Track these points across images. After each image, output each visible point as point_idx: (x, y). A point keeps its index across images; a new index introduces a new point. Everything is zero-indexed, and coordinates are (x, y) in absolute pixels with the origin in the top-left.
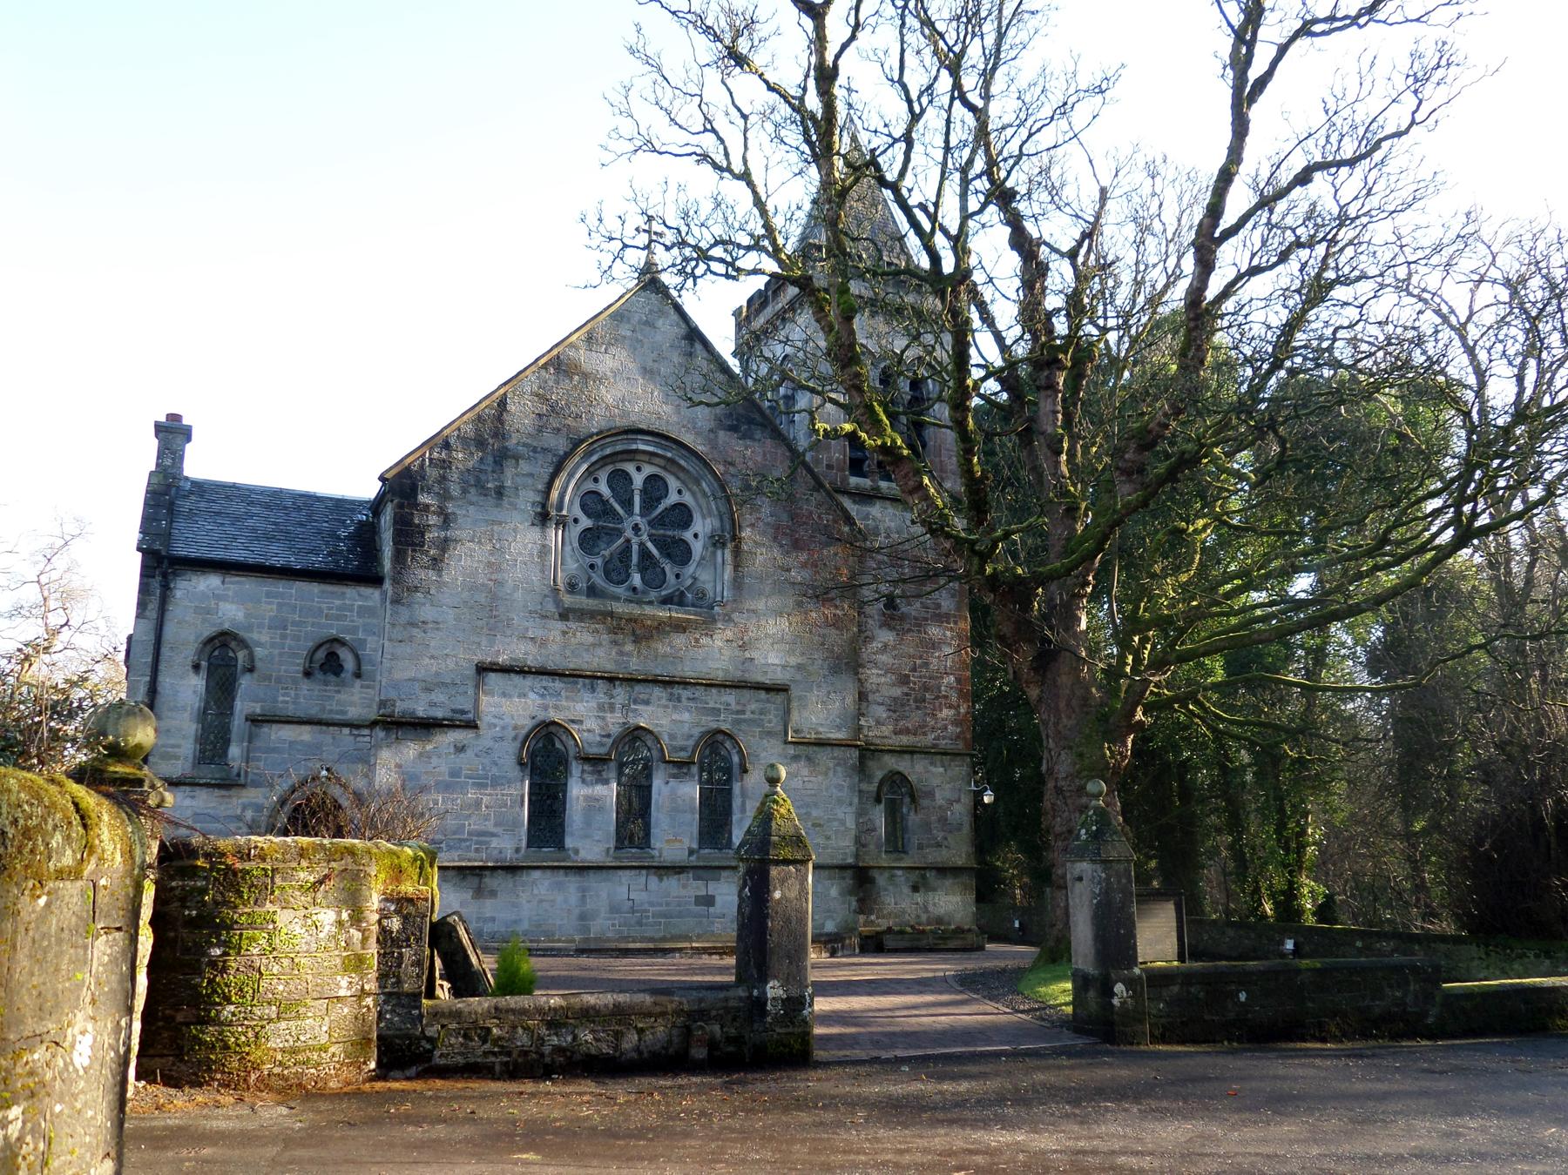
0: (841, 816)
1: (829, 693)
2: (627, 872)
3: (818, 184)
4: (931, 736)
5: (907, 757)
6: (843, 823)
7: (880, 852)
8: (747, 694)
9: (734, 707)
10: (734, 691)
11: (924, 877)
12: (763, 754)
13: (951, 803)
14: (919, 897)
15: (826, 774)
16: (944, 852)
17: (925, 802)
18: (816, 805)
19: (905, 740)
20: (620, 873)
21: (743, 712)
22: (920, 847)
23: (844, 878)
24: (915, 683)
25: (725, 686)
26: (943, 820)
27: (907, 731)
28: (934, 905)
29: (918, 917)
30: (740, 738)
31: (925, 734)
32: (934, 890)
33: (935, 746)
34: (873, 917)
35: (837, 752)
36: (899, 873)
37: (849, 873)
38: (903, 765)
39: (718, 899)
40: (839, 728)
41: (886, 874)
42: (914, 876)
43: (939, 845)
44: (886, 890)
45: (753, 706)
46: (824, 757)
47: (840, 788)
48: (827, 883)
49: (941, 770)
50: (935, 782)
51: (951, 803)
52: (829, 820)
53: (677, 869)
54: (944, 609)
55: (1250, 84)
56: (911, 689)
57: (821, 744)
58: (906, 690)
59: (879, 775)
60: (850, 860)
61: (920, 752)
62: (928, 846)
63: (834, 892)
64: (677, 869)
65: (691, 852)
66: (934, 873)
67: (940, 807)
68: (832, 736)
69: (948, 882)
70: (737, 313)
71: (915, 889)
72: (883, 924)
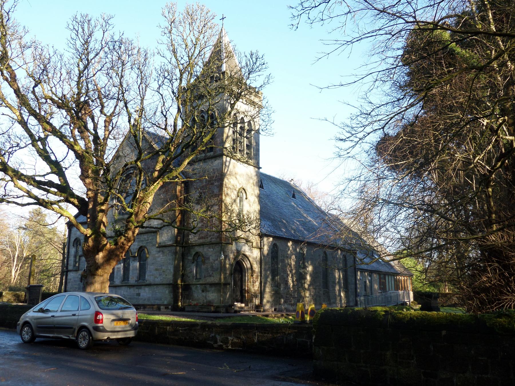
0: (170, 268)
1: (168, 230)
2: (124, 287)
3: (39, 197)
4: (209, 238)
5: (202, 246)
6: (170, 270)
7: (193, 279)
8: (149, 234)
9: (146, 239)
10: (146, 234)
11: (206, 287)
12: (152, 252)
13: (215, 261)
14: (204, 294)
15: (167, 256)
16: (212, 278)
17: (207, 261)
18: (164, 265)
19: (201, 241)
20: (122, 287)
21: (148, 240)
22: (205, 277)
23: (169, 288)
24: (205, 221)
25: (144, 233)
26: (212, 267)
27: (202, 238)
28: (208, 296)
29: (203, 300)
30: (148, 247)
31: (207, 238)
32: (209, 291)
33: (211, 241)
34: (191, 301)
35: (169, 248)
36: (198, 286)
37: (171, 286)
38: (198, 249)
39: (141, 294)
40: (170, 241)
41: (195, 287)
42: (203, 287)
43: (210, 276)
44: (195, 292)
45: (150, 238)
46: (166, 250)
47: (170, 259)
48: (165, 289)
49: (212, 249)
50: (210, 254)
51: (215, 261)
52: (167, 270)
53: (133, 286)
54: (215, 193)
55: (49, 188)
56: (205, 223)
57: (165, 246)
58: (202, 224)
59: (194, 253)
60: (171, 282)
61: (205, 244)
62: (207, 277)
63: (167, 292)
64: (133, 286)
65: (136, 281)
66: (209, 286)
67: (211, 263)
68: (168, 243)
69: (213, 289)
70: (80, 177)
71: (203, 291)
72: (194, 303)
